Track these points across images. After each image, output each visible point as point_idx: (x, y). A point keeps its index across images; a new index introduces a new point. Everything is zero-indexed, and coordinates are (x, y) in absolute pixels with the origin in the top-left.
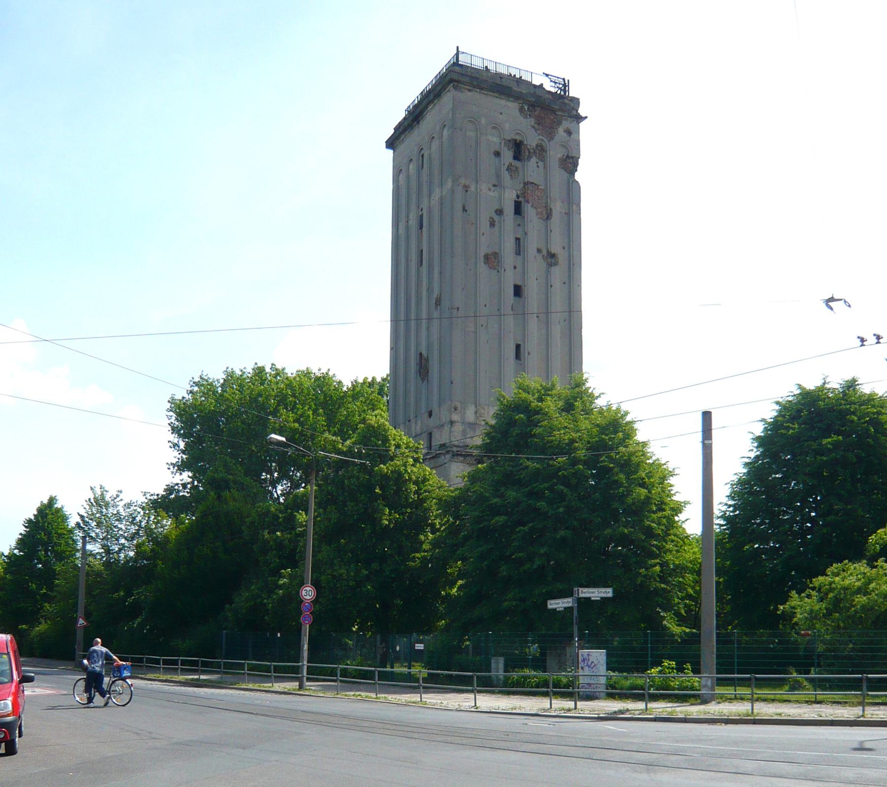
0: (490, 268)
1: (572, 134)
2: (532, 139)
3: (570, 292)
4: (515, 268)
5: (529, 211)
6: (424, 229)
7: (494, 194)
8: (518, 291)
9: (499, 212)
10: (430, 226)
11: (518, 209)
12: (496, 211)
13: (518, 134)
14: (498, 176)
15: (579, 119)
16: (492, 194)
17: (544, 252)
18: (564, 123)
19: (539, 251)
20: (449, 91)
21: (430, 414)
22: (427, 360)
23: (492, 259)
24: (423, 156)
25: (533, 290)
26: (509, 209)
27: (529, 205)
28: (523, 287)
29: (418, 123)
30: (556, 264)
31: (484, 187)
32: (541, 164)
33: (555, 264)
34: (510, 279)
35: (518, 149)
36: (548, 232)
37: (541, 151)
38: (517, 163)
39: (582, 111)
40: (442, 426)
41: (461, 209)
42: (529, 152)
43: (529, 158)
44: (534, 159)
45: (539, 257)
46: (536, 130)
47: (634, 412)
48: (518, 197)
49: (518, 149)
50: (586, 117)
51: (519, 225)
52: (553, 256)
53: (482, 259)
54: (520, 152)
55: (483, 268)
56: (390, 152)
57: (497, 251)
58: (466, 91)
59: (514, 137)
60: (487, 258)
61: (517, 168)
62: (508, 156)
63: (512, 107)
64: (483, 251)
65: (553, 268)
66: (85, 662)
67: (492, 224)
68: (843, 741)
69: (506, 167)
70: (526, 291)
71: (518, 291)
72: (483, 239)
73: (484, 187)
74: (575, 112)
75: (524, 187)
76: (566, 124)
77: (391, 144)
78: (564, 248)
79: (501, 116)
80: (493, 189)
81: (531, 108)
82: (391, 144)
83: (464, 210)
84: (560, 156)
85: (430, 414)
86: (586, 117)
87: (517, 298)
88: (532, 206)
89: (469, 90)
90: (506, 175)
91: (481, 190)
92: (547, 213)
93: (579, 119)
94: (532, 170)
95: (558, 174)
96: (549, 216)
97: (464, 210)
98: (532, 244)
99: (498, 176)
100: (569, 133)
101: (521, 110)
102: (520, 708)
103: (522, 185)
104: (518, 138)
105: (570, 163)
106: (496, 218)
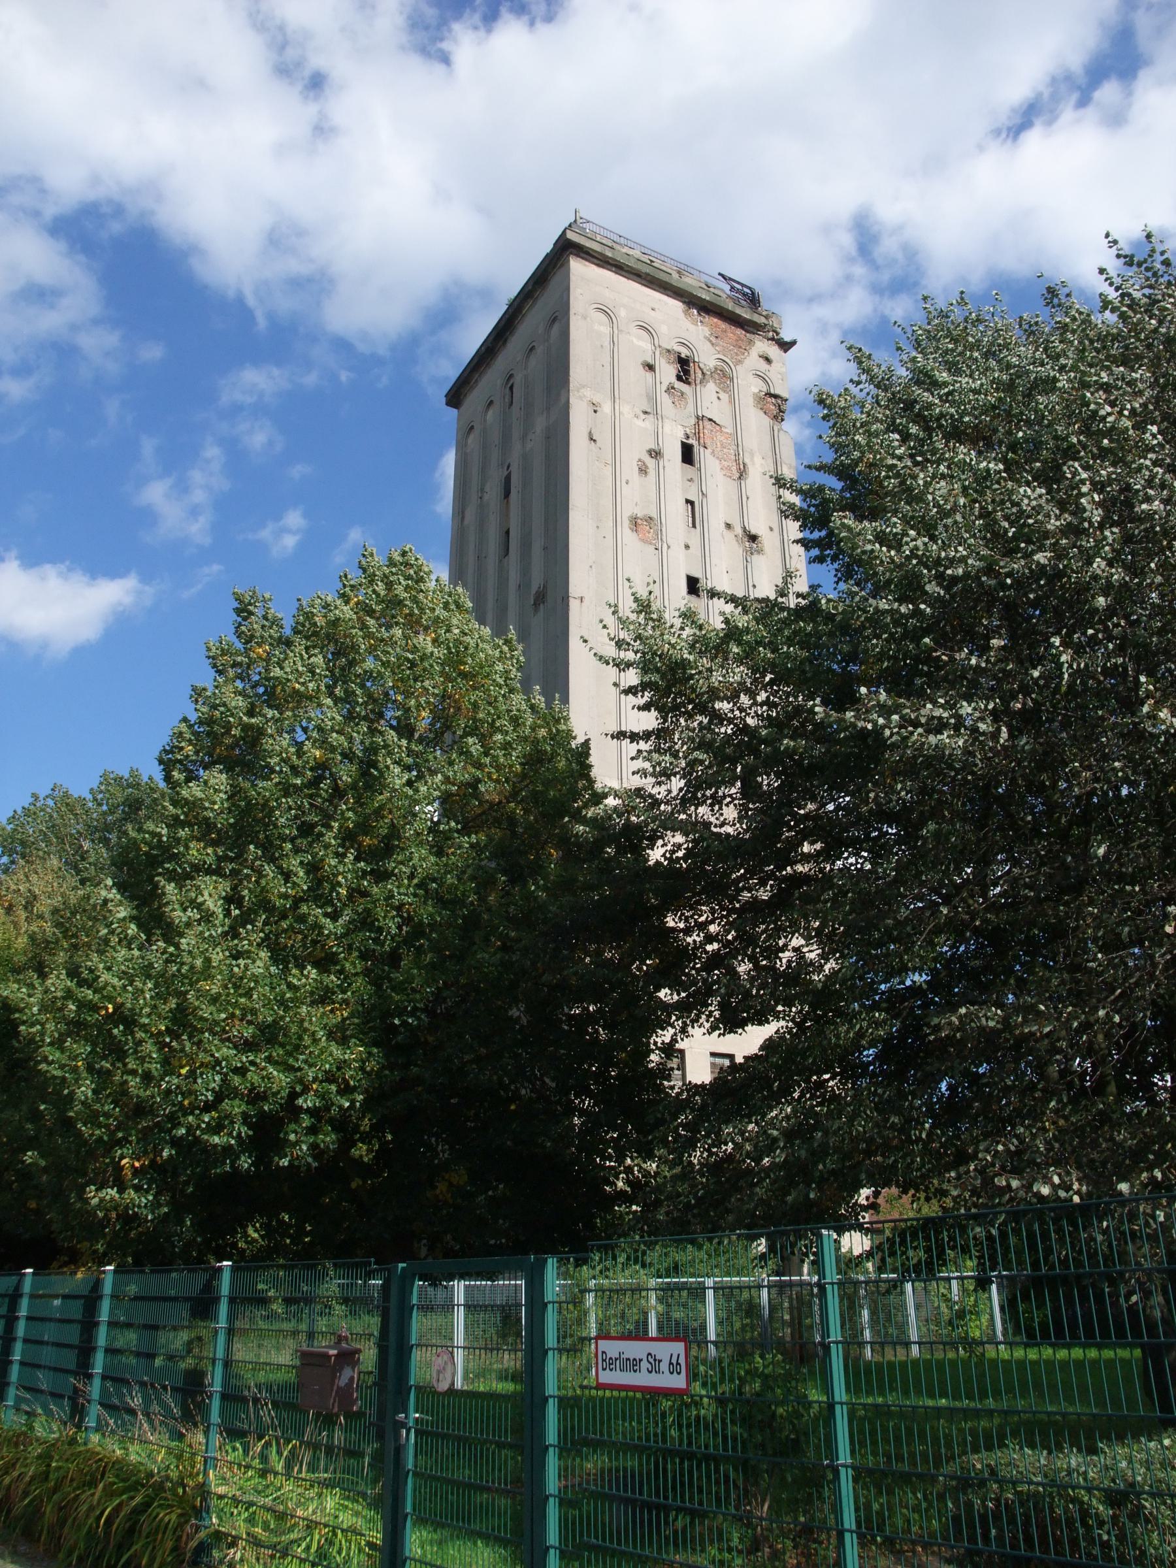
0: (642, 540)
2: (707, 357)
4: (687, 547)
6: (515, 407)
7: (648, 424)
9: (656, 454)
10: (526, 546)
11: (688, 455)
14: (653, 399)
16: (639, 423)
17: (739, 531)
24: (511, 388)
26: (674, 453)
27: (708, 452)
29: (505, 341)
30: (760, 551)
36: (742, 501)
37: (724, 377)
44: (711, 387)
47: (1155, 223)
49: (685, 367)
52: (753, 538)
53: (626, 523)
54: (687, 372)
55: (628, 536)
56: (454, 412)
57: (654, 515)
62: (668, 372)
67: (643, 470)
69: (664, 388)
90: (665, 400)
96: (742, 474)
98: (718, 510)
99: (653, 399)
103: (693, 421)
104: (684, 353)
106: (651, 463)
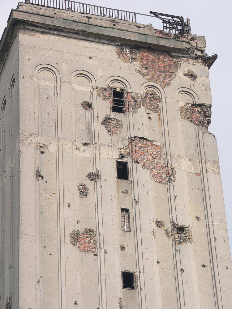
0: (81, 250)
2: (136, 85)
3: (214, 276)
4: (123, 248)
5: (137, 171)
8: (128, 280)
9: (94, 177)
11: (123, 172)
14: (90, 131)
16: (81, 154)
17: (168, 226)
18: (184, 65)
19: (159, 224)
23: (84, 239)
25: (151, 279)
28: (137, 275)
30: (188, 240)
31: (68, 146)
32: (154, 115)
33: (186, 241)
34: (114, 266)
35: (119, 100)
37: (152, 100)
38: (114, 115)
41: (33, 173)
43: (135, 109)
44: (142, 111)
45: (160, 232)
46: (143, 75)
48: (122, 156)
49: (119, 100)
51: (125, 192)
53: (69, 239)
55: (71, 252)
60: (76, 237)
61: (118, 121)
62: (104, 107)
64: (70, 228)
67: (84, 192)
68: (6, 155)
69: (101, 120)
70: (140, 280)
71: (128, 280)
72: (69, 212)
73: (68, 146)
75: (130, 144)
78: (198, 218)
79: (90, 61)
80: (83, 148)
83: (39, 175)
84: (182, 104)
87: (128, 291)
88: (144, 167)
91: (63, 150)
94: (139, 121)
96: (171, 177)
97: (39, 175)
98: (148, 212)
99: (90, 131)
103: (127, 142)
104: (118, 87)
106: (90, 184)
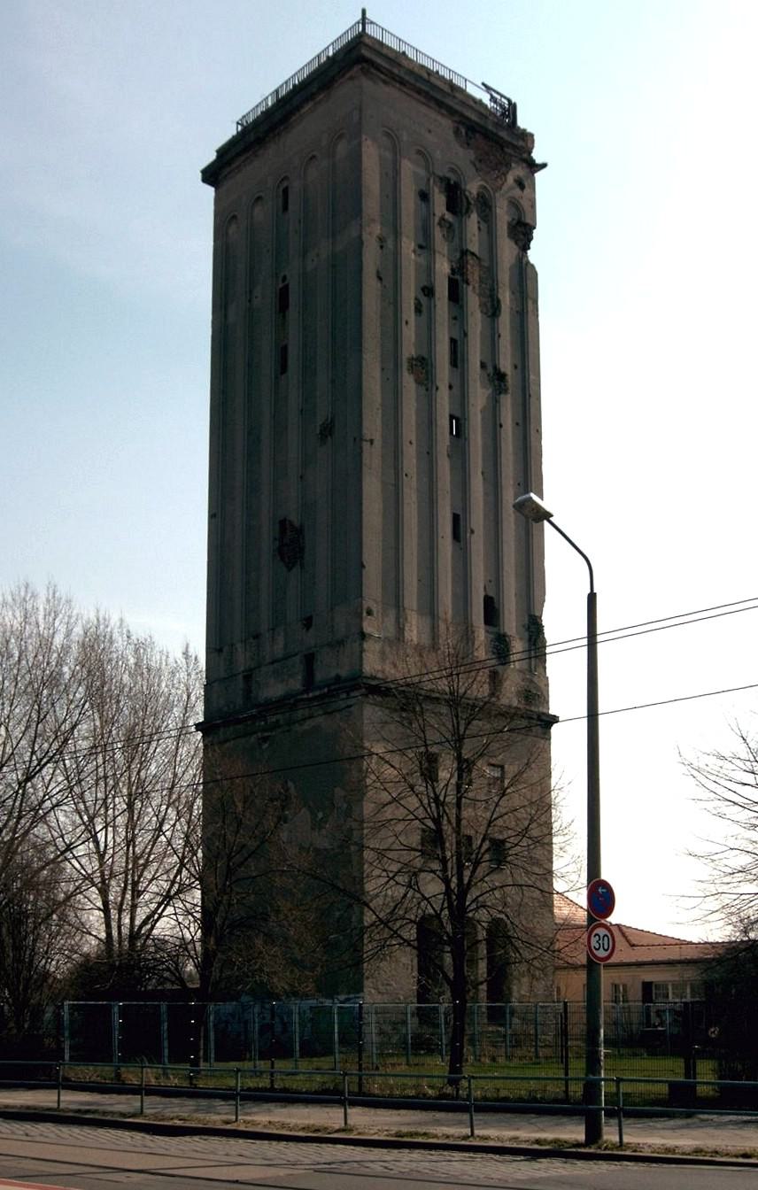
1: (525, 185)
6: (293, 313)
12: (423, 289)
13: (452, 170)
15: (534, 167)
20: (351, 78)
21: (308, 623)
22: (300, 531)
24: (286, 191)
37: (485, 206)
39: (538, 156)
40: (341, 643)
42: (469, 203)
50: (544, 166)
57: (426, 356)
58: (381, 84)
59: (449, 175)
63: (446, 124)
65: (502, 396)
66: (723, 1051)
67: (418, 310)
74: (525, 156)
75: (461, 258)
76: (518, 171)
77: (211, 175)
78: (516, 367)
81: (470, 133)
82: (211, 175)
85: (308, 623)
86: (544, 166)
89: (385, 82)
92: (493, 305)
93: (534, 167)
95: (507, 249)
100: (520, 184)
101: (457, 132)
102: (283, 1126)
103: (458, 255)
105: (523, 231)
106: (424, 300)
